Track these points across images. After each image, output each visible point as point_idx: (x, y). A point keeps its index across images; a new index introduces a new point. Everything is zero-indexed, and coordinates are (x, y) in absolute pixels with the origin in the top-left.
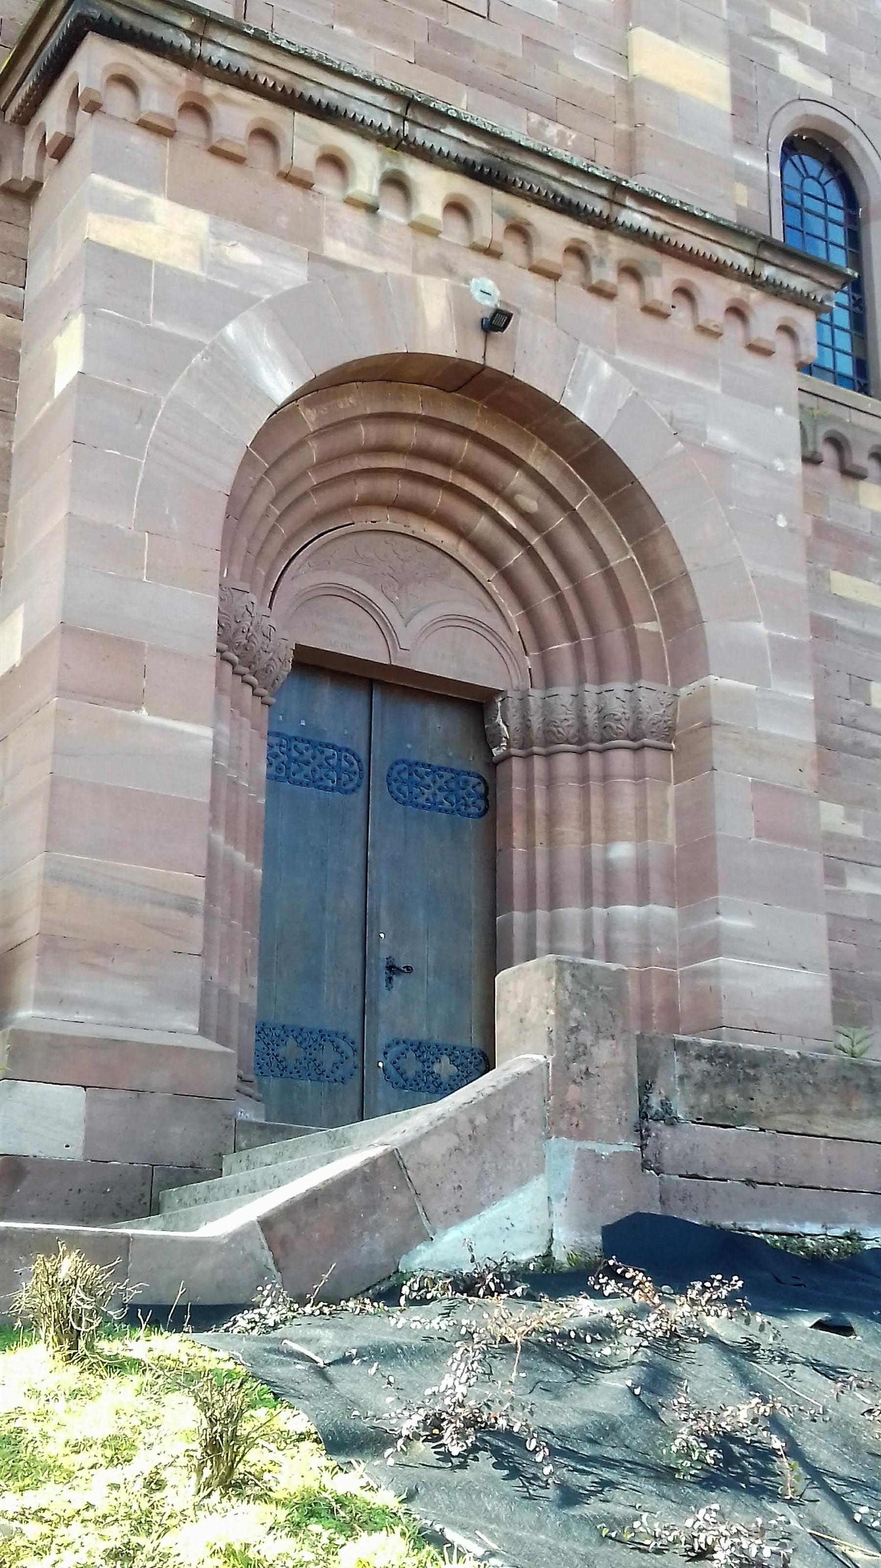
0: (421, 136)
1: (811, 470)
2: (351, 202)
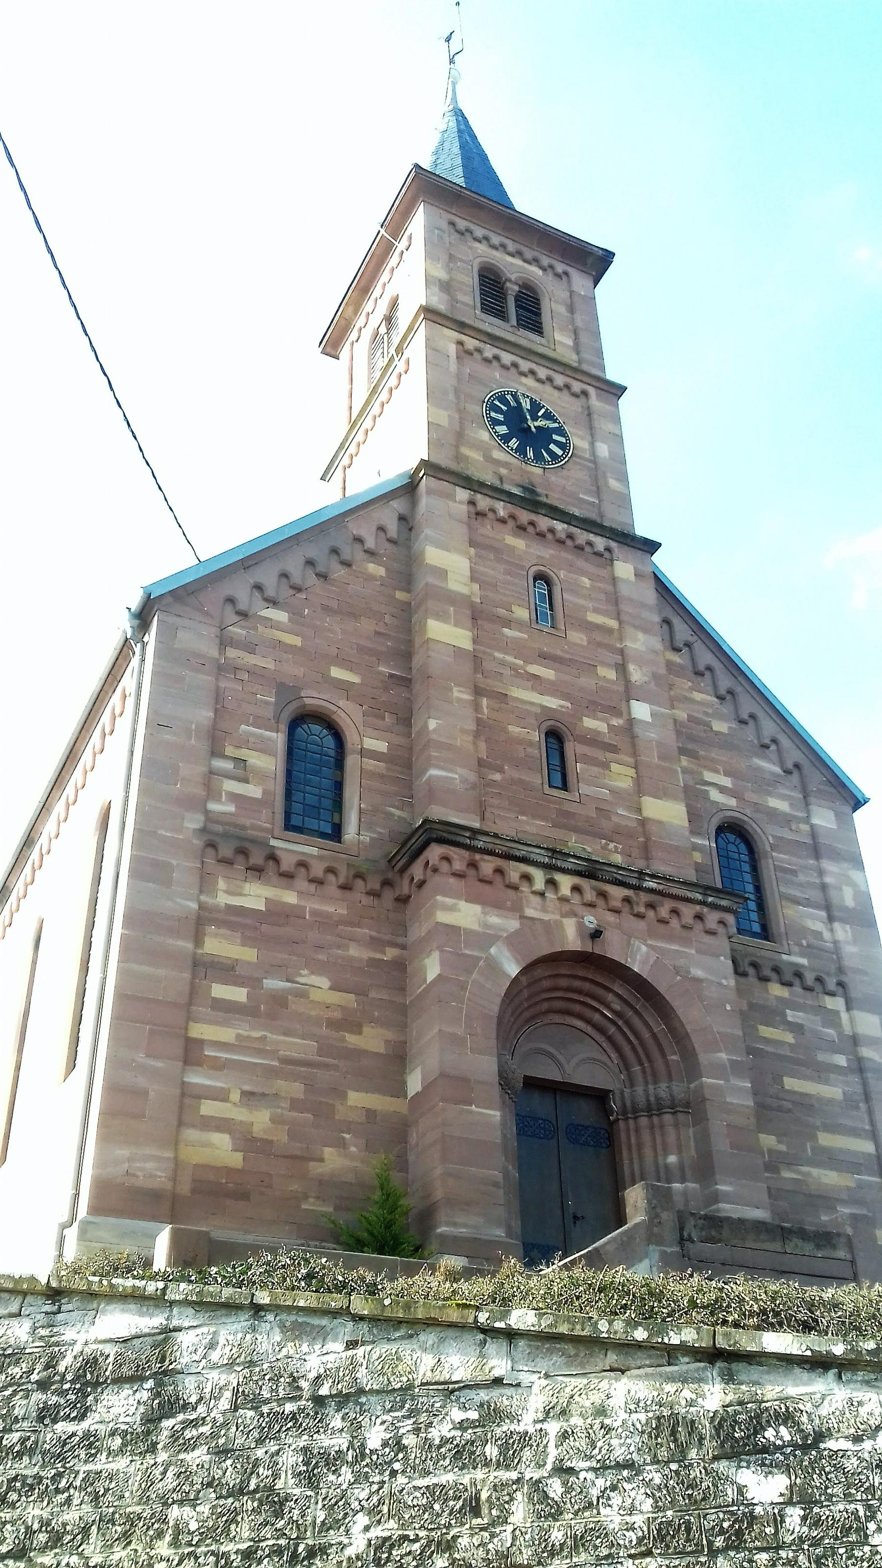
0: (559, 863)
1: (742, 980)
2: (534, 893)
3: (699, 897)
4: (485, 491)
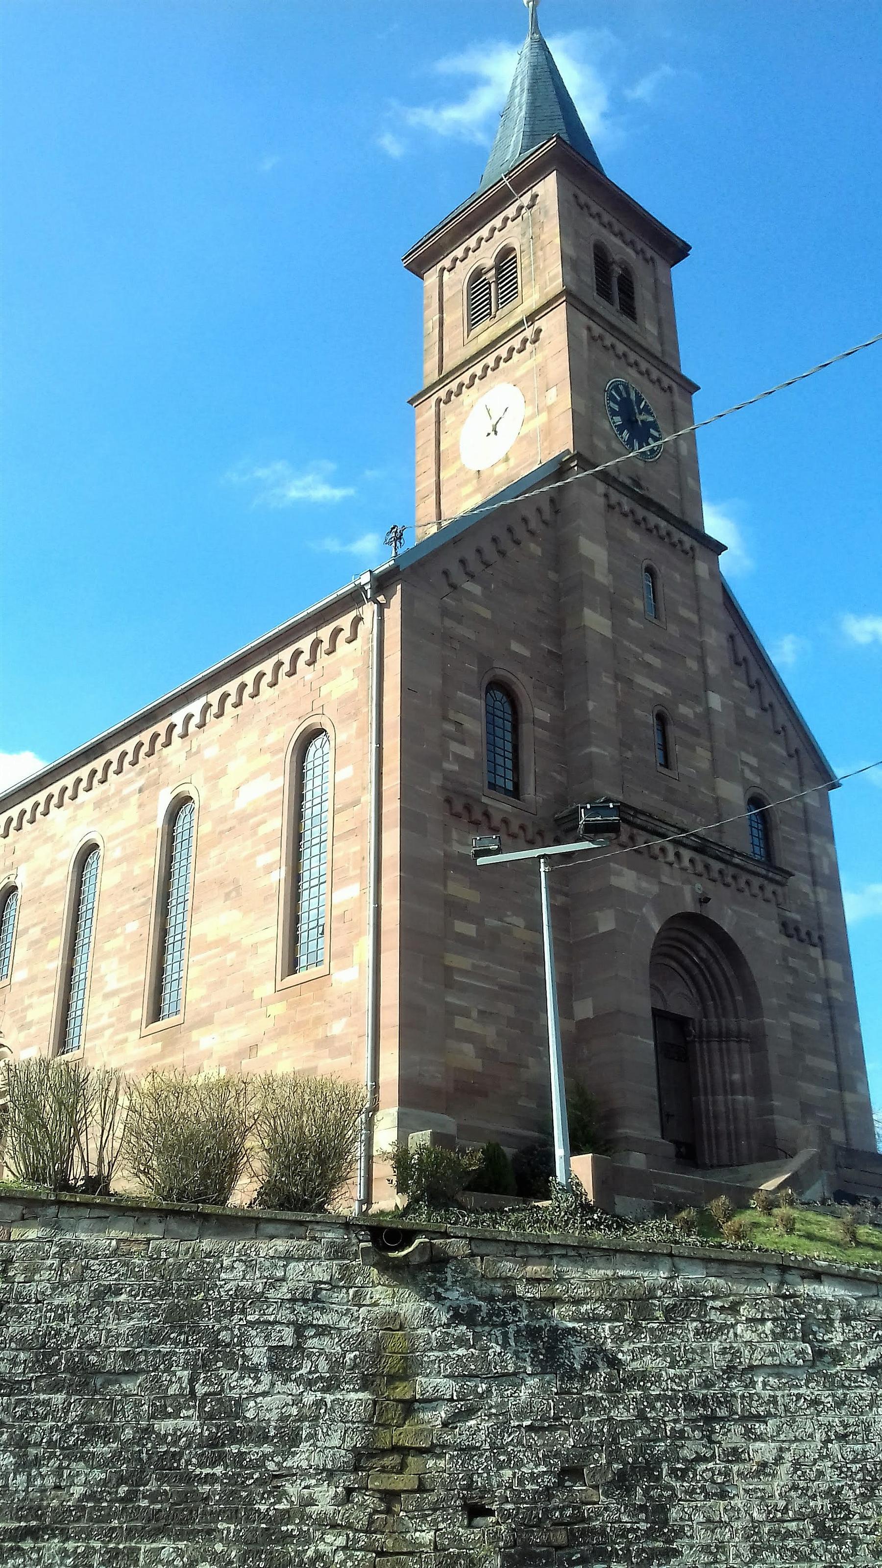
2: (667, 863)
3: (764, 872)
4: (616, 486)
